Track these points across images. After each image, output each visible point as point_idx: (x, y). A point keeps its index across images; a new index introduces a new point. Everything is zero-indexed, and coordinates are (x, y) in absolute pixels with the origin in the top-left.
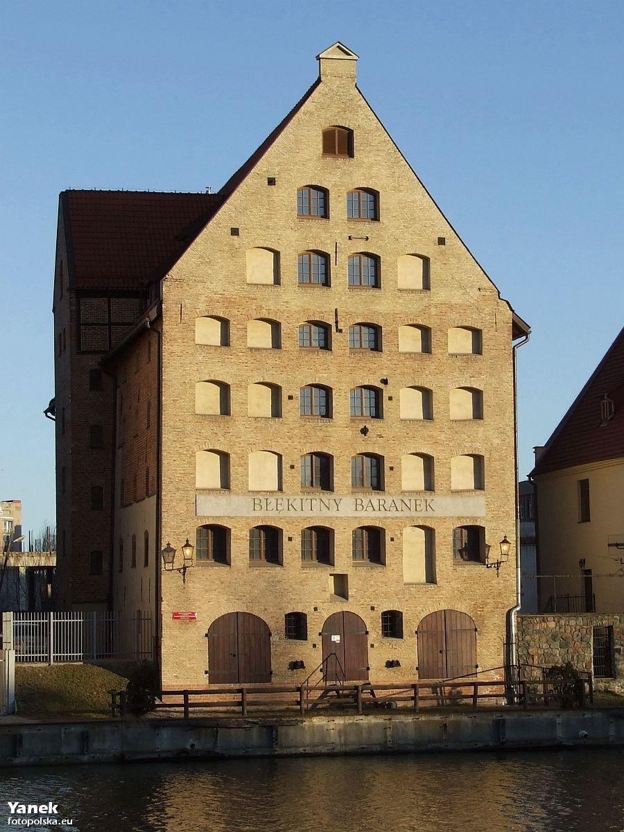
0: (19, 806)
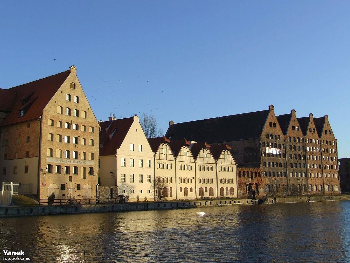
0: (8, 252)
